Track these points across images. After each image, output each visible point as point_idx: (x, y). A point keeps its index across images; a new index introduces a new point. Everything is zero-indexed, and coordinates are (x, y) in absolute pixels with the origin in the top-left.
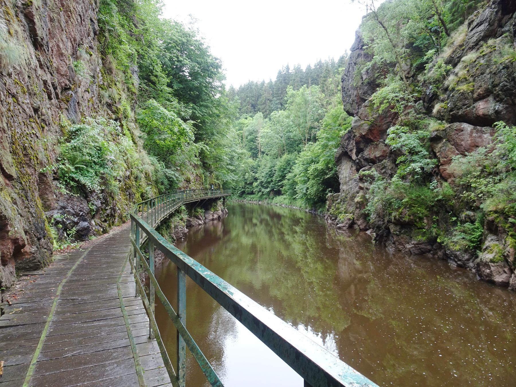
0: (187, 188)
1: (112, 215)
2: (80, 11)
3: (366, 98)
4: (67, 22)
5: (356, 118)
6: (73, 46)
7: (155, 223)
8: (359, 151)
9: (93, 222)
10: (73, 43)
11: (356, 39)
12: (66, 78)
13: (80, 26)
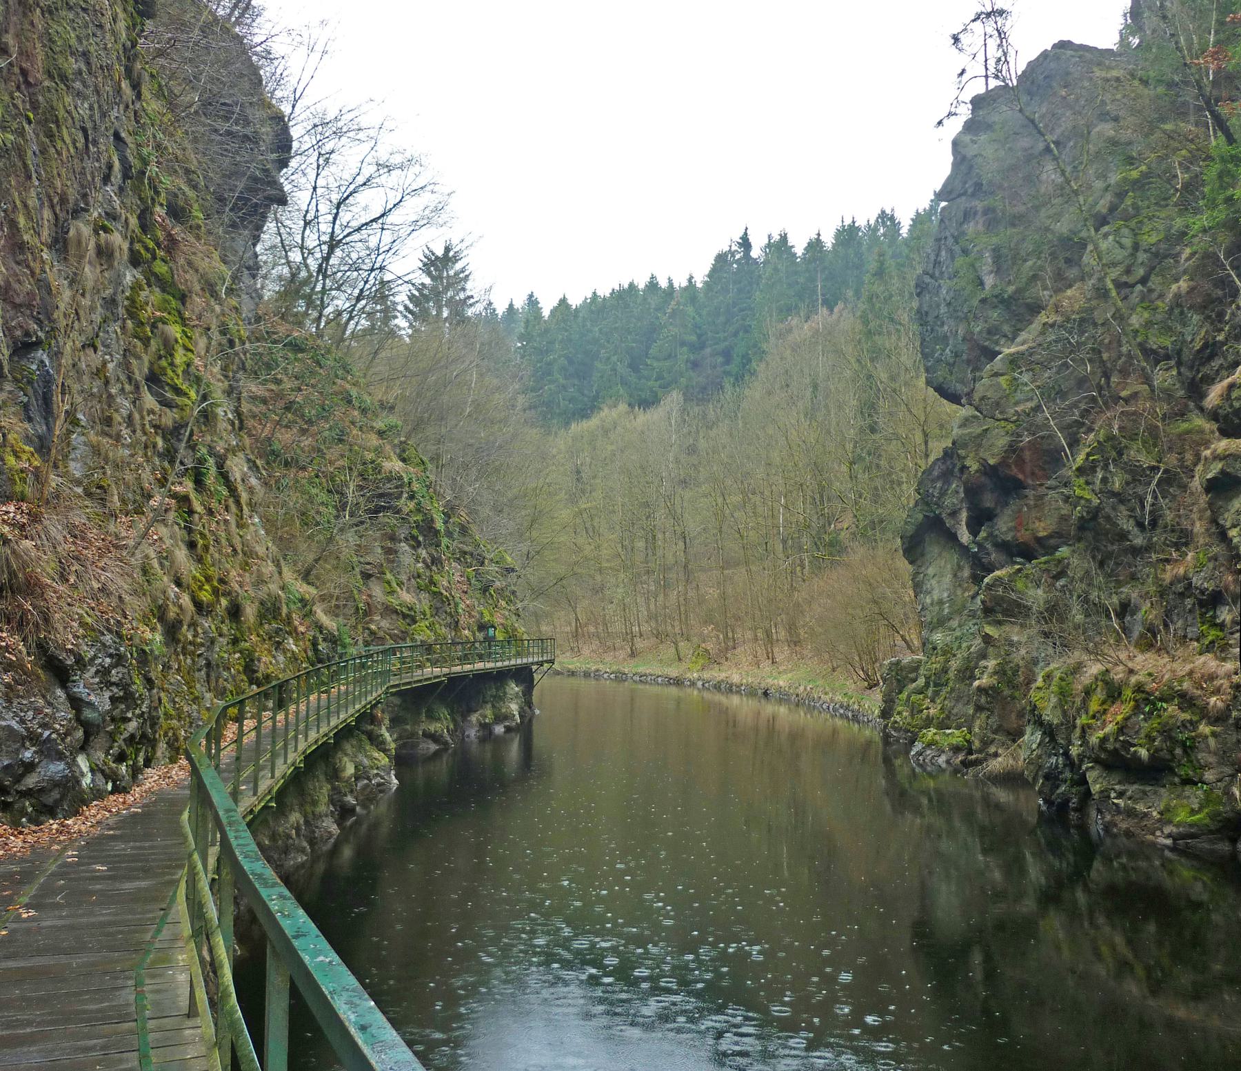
0: (404, 639)
1: (144, 736)
2: (86, 117)
3: (997, 349)
4: (43, 151)
5: (965, 411)
6: (57, 218)
7: (296, 750)
8: (979, 519)
9: (83, 762)
10: (58, 209)
11: (956, 165)
12: (28, 312)
13: (82, 160)
